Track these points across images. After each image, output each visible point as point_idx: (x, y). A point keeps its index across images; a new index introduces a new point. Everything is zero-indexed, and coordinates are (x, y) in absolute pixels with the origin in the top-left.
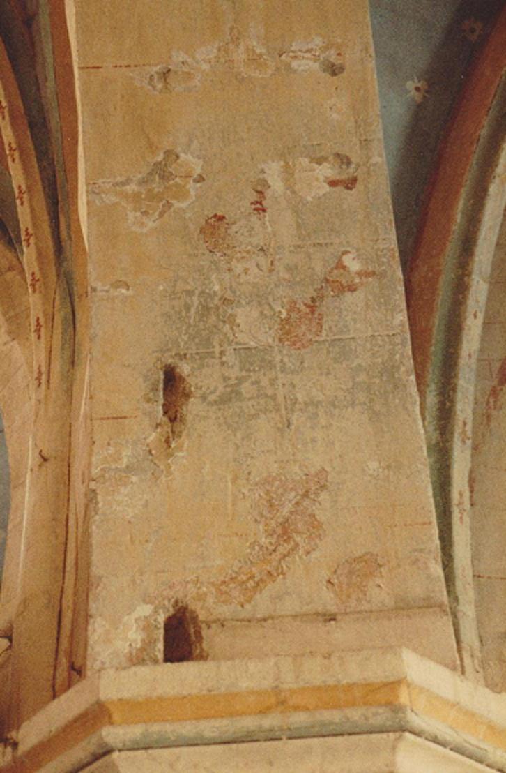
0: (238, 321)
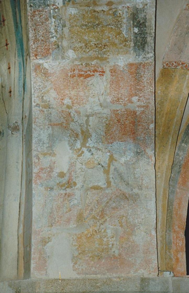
0: (90, 124)
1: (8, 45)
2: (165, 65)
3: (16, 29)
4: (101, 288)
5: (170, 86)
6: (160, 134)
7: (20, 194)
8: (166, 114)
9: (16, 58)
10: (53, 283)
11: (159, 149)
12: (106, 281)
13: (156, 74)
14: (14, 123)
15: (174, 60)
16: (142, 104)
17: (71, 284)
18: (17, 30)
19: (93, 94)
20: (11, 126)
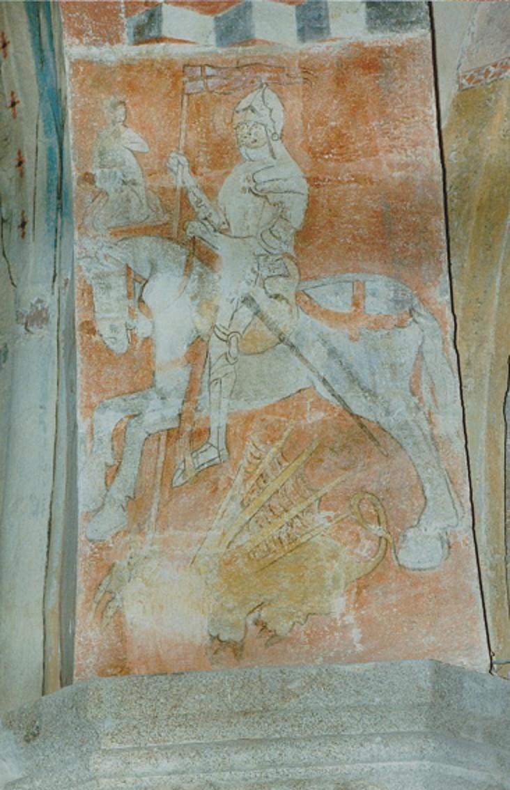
1: (17, 106)
2: (464, 81)
3: (40, 65)
4: (301, 697)
5: (484, 130)
6: (465, 265)
7: (52, 496)
8: (478, 210)
9: (40, 138)
10: (144, 687)
11: (463, 309)
12: (318, 674)
13: (442, 108)
14: (33, 302)
15: (488, 63)
16: (402, 159)
17: (203, 689)
18: (42, 69)
19: (252, 136)
20: (26, 312)
